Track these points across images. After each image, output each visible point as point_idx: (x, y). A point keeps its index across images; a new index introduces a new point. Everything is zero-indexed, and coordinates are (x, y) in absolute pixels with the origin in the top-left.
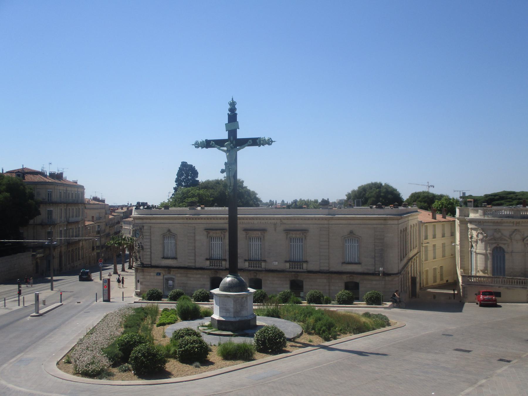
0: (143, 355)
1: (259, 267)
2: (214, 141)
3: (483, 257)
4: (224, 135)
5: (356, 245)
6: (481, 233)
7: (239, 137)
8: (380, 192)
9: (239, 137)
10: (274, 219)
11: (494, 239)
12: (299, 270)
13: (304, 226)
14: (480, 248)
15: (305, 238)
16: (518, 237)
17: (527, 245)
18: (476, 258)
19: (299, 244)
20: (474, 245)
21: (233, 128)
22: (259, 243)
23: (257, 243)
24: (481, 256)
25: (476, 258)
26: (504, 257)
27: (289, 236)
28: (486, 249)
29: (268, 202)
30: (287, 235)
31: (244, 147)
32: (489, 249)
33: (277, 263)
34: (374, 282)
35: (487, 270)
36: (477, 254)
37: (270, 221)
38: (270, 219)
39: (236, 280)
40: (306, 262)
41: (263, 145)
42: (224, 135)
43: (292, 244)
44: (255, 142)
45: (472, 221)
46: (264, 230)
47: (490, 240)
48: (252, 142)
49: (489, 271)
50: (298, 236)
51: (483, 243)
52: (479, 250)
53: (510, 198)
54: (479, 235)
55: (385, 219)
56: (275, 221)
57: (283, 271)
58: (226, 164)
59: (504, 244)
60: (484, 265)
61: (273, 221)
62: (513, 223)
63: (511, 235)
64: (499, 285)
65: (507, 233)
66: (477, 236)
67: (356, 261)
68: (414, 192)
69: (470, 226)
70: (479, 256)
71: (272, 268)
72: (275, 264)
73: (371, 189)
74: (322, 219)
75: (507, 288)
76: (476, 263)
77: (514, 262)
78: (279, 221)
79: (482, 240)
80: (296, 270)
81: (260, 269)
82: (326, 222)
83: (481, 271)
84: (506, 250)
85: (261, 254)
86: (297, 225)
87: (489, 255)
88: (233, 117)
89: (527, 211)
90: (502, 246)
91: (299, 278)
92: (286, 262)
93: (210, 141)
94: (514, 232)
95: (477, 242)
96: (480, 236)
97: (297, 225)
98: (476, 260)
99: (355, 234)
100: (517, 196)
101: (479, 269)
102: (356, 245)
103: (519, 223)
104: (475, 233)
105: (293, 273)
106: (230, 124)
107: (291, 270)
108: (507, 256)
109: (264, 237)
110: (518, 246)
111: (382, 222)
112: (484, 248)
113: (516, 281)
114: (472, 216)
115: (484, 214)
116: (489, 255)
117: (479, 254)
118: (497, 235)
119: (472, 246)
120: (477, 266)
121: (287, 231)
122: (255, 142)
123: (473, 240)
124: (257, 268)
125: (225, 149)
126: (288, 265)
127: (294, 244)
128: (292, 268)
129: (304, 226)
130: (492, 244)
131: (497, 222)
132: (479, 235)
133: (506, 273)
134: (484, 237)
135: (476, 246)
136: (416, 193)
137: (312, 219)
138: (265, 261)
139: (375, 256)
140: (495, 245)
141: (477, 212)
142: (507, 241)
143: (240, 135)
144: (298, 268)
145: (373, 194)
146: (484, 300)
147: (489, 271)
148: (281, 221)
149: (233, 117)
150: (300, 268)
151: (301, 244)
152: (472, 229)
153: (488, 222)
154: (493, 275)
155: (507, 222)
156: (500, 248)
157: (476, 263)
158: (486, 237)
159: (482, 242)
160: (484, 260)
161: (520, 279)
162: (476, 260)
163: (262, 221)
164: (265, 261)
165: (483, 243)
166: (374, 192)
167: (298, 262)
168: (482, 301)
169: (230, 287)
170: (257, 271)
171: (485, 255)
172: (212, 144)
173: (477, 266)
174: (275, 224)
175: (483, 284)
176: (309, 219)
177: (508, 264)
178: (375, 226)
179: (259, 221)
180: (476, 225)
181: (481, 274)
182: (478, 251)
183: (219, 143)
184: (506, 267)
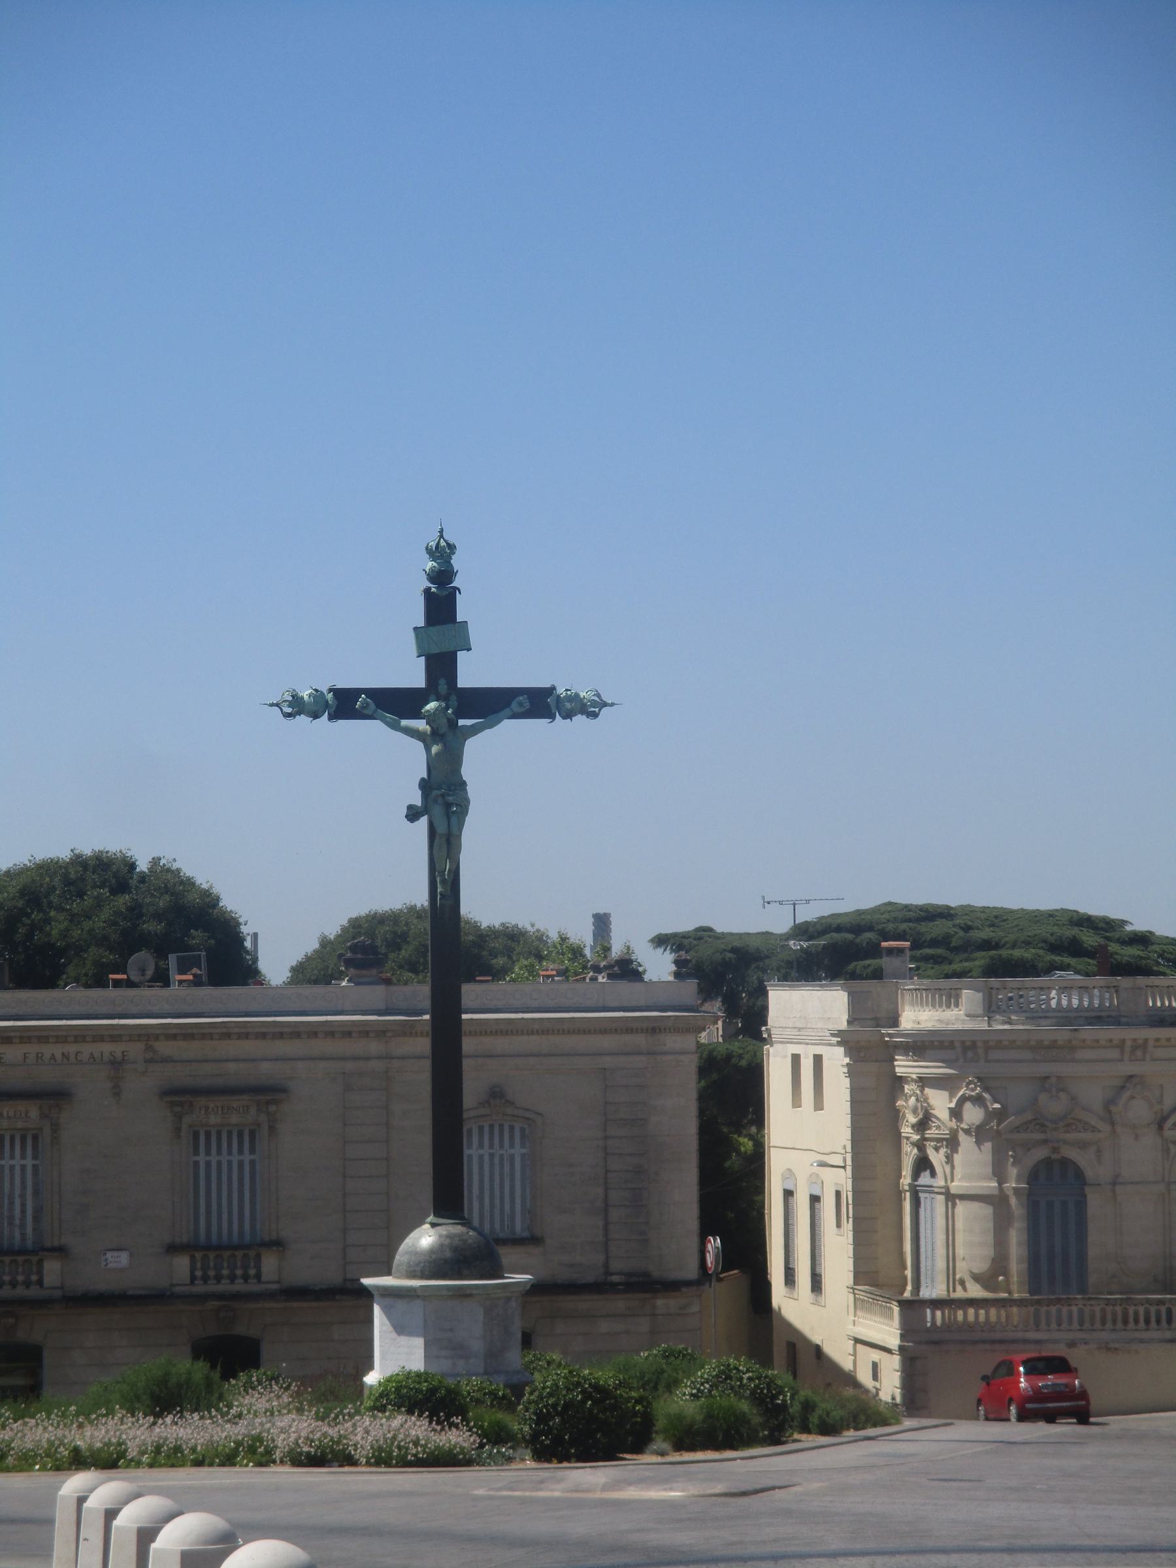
0: (587, 1395)
1: (27, 1284)
2: (372, 693)
3: (987, 1210)
4: (411, 674)
5: (518, 1151)
6: (978, 1100)
7: (463, 682)
8: (135, 911)
9: (463, 682)
10: (115, 1036)
11: (1039, 1122)
12: (239, 1286)
13: (266, 1071)
14: (968, 1168)
15: (272, 1129)
16: (1139, 1110)
17: (1172, 1147)
18: (950, 1218)
19: (235, 1159)
20: (937, 1158)
21: (445, 647)
22: (29, 1162)
23: (17, 1162)
24: (975, 1206)
25: (950, 1218)
26: (1081, 1205)
27: (187, 1120)
28: (999, 1173)
29: (554, 936)
30: (179, 1117)
31: (499, 721)
32: (1013, 1172)
33: (123, 1259)
34: (604, 1326)
35: (1005, 1272)
36: (951, 1198)
37: (87, 1049)
38: (99, 1036)
39: (459, 1229)
40: (277, 1244)
41: (568, 715)
42: (411, 674)
43: (202, 1158)
44: (539, 703)
45: (922, 1045)
46: (55, 1097)
47: (1017, 1129)
48: (527, 705)
49: (1015, 1279)
50: (234, 1119)
51: (988, 1146)
52: (962, 1179)
53: (934, 943)
54: (968, 1106)
55: (654, 1029)
56: (118, 1049)
57: (157, 1298)
58: (425, 785)
59: (1083, 1145)
60: (989, 1252)
61: (107, 1048)
62: (1121, 1046)
63: (1109, 1104)
64: (1070, 1336)
65: (1093, 1095)
66: (956, 1113)
67: (518, 1227)
68: (361, 909)
69: (904, 1066)
70: (961, 1208)
71: (101, 1284)
72: (117, 1266)
73: (81, 894)
74: (349, 1034)
75: (1107, 1348)
76: (950, 1244)
77: (1122, 1231)
78: (135, 1050)
79: (980, 1133)
80: (225, 1287)
81: (33, 1292)
82: (374, 1047)
83: (976, 1278)
84: (1089, 1173)
85: (37, 1218)
86: (232, 1067)
87: (1013, 1201)
88: (441, 604)
89: (1170, 991)
90: (1072, 1154)
91: (241, 1329)
92: (173, 1249)
93: (353, 694)
94: (1123, 1087)
95: (952, 1143)
96: (973, 1115)
97: (232, 1067)
98: (950, 1231)
99: (511, 1103)
100: (967, 928)
101: (962, 1269)
102: (518, 1151)
103: (1143, 1046)
104: (940, 1103)
105: (213, 1304)
106: (433, 630)
107: (200, 1288)
108: (1095, 1202)
109: (55, 1128)
110: (1139, 1155)
111: (640, 1040)
112: (989, 1170)
113: (1141, 1310)
114: (917, 1016)
115: (991, 1008)
116: (1013, 1201)
117: (963, 1197)
118: (1054, 1106)
119: (923, 1164)
120: (951, 1259)
121: (180, 1097)
122: (539, 703)
123: (930, 1133)
124: (20, 1291)
125: (421, 725)
126: (182, 1263)
127: (214, 1159)
128: (205, 1278)
129: (266, 1067)
130: (1028, 1146)
131: (1053, 1045)
132: (968, 1106)
133: (1092, 1279)
134: (990, 1115)
135: (949, 1159)
136: (376, 920)
137: (313, 1032)
138: (60, 1251)
139: (607, 1205)
140: (1041, 1153)
141: (952, 999)
142: (1094, 1129)
143: (472, 673)
144: (232, 1278)
145: (99, 922)
146: (1038, 1396)
147: (1015, 1279)
148: (149, 1048)
149: (441, 604)
150: (246, 1278)
151: (247, 1157)
152: (923, 1082)
153: (1012, 1045)
154: (1032, 1293)
155: (1096, 1044)
156: (1065, 1162)
157: (950, 1244)
158: (1001, 1115)
159: (979, 1143)
160: (991, 1225)
161: (1160, 1302)
162: (950, 1231)
163: (48, 1050)
164: (60, 1251)
165: (988, 1146)
166: (106, 913)
167: (236, 1248)
168: (1030, 1399)
169: (440, 1264)
170: (23, 1302)
171: (997, 1201)
172: (365, 706)
173: (951, 1259)
174: (117, 1064)
175: (998, 1336)
176: (296, 1032)
177: (1099, 1240)
178: (608, 1061)
179: (32, 1049)
180: (949, 1063)
181: (975, 1291)
182: (956, 1186)
183: (393, 704)
184: (1092, 1252)
